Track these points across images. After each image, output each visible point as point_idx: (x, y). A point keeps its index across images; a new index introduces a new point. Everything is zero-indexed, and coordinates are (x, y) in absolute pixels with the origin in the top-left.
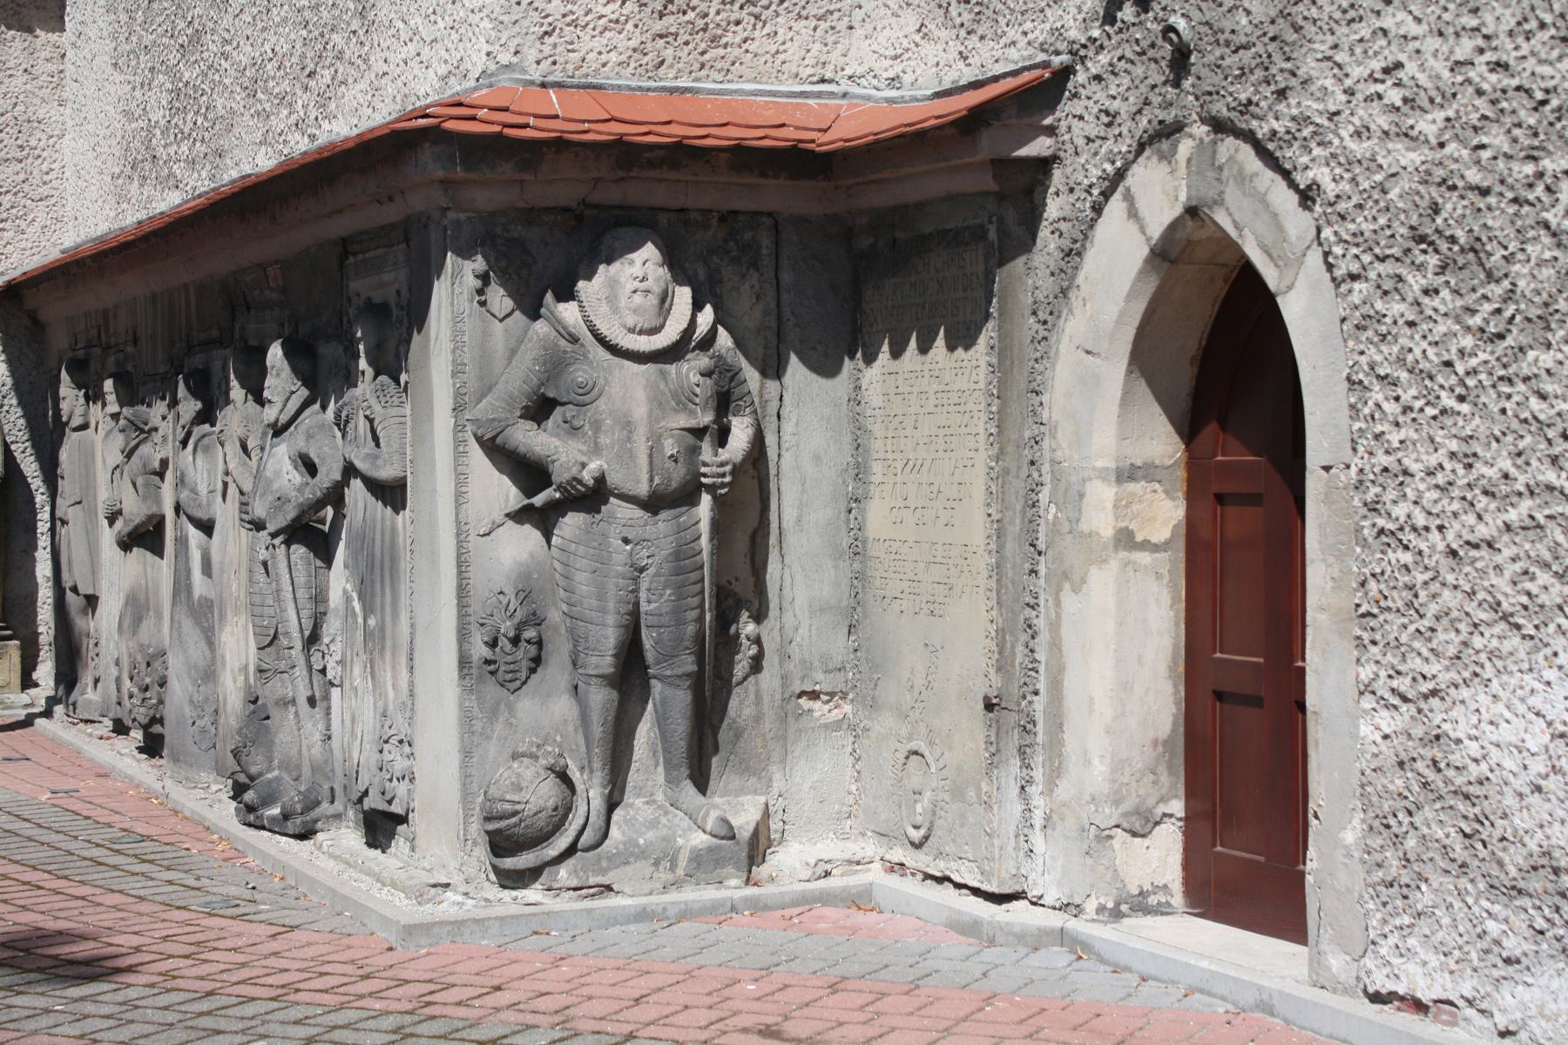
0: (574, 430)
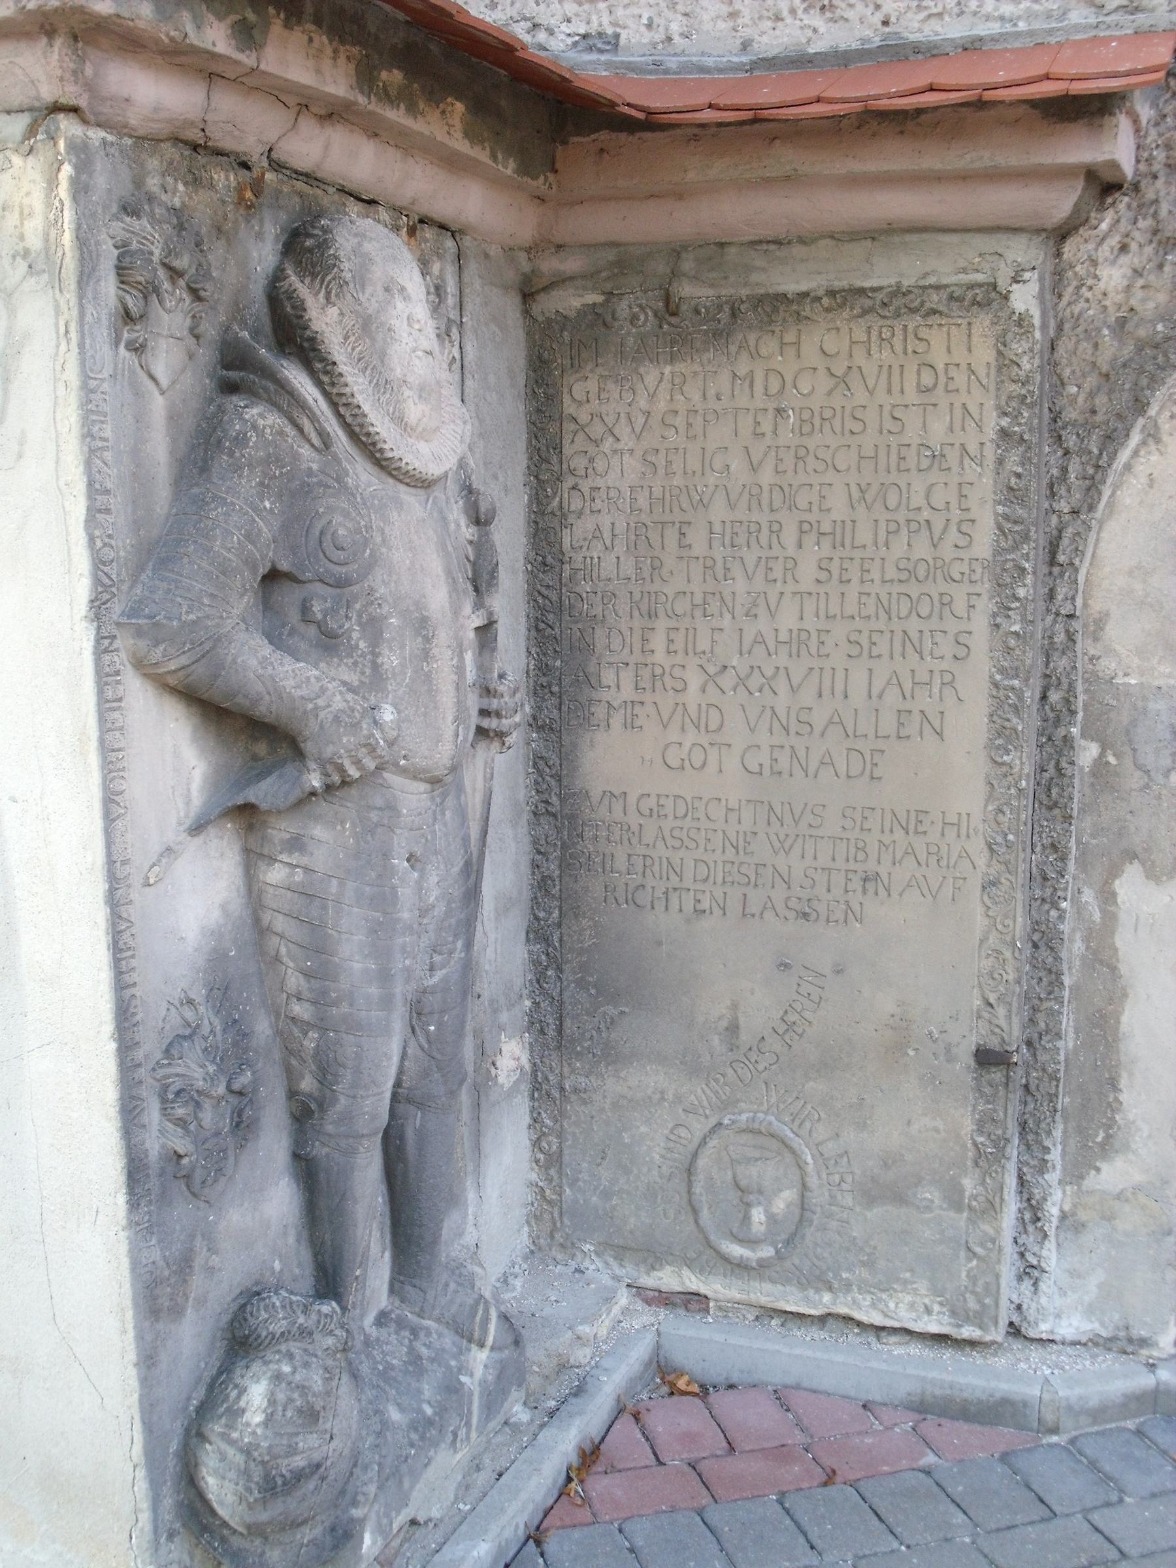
0: (329, 642)
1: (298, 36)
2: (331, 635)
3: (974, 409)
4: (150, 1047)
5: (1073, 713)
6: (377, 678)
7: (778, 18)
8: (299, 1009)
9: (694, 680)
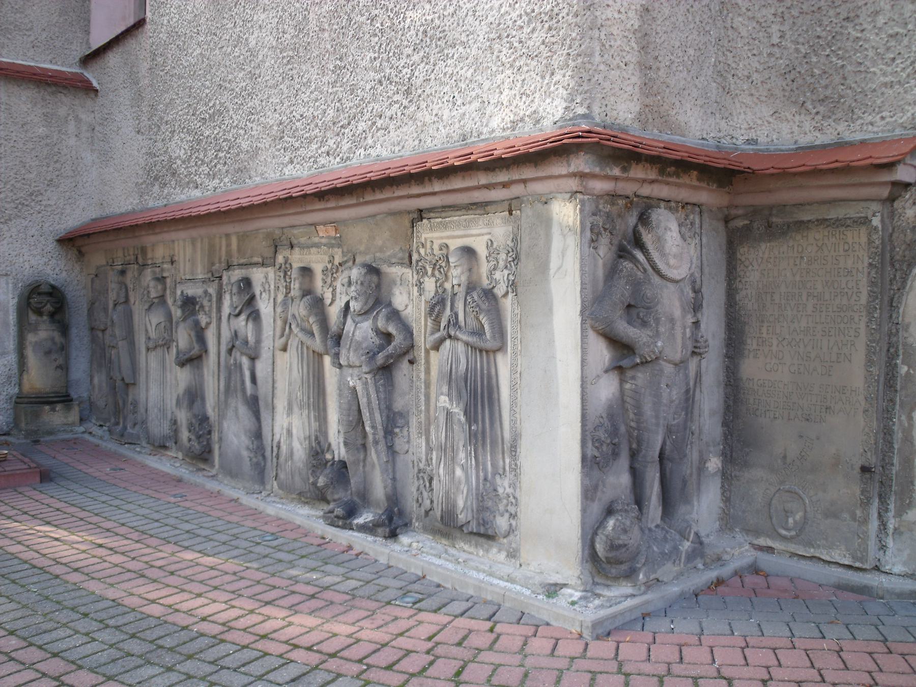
0: (644, 324)
1: (640, 166)
2: (645, 322)
3: (860, 256)
4: (590, 426)
5: (898, 356)
6: (657, 334)
7: (806, 134)
8: (633, 424)
9: (775, 342)
